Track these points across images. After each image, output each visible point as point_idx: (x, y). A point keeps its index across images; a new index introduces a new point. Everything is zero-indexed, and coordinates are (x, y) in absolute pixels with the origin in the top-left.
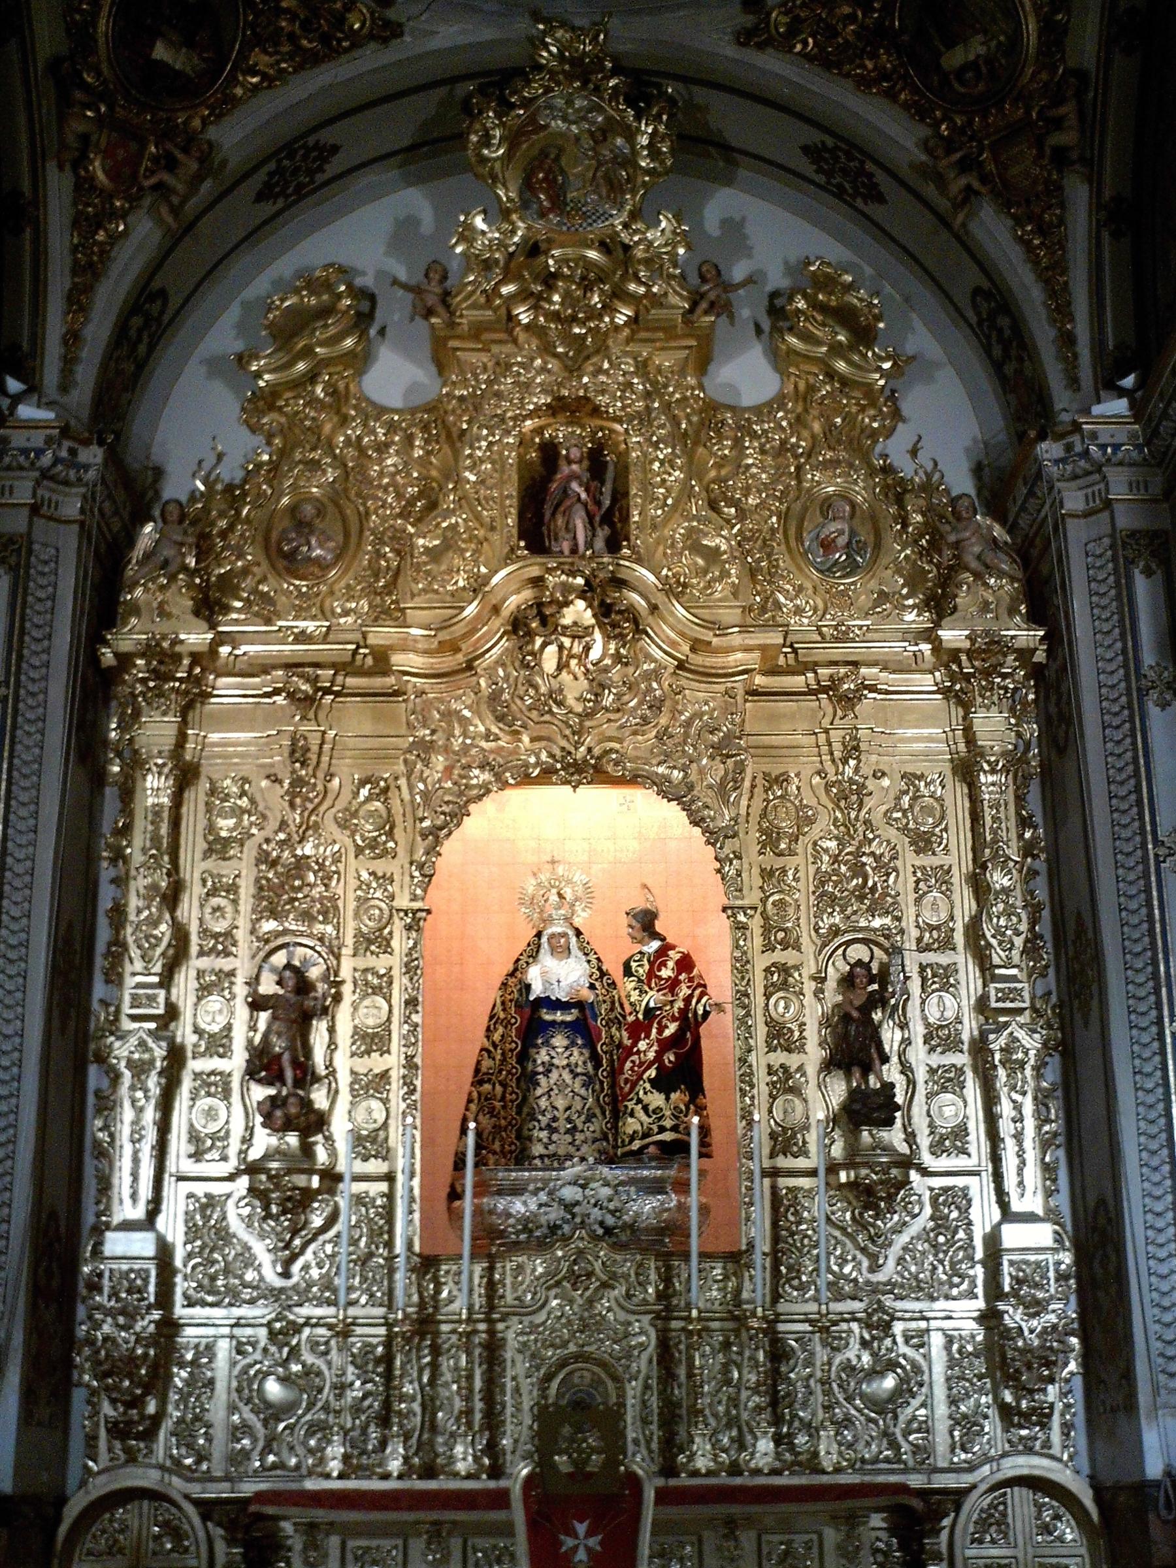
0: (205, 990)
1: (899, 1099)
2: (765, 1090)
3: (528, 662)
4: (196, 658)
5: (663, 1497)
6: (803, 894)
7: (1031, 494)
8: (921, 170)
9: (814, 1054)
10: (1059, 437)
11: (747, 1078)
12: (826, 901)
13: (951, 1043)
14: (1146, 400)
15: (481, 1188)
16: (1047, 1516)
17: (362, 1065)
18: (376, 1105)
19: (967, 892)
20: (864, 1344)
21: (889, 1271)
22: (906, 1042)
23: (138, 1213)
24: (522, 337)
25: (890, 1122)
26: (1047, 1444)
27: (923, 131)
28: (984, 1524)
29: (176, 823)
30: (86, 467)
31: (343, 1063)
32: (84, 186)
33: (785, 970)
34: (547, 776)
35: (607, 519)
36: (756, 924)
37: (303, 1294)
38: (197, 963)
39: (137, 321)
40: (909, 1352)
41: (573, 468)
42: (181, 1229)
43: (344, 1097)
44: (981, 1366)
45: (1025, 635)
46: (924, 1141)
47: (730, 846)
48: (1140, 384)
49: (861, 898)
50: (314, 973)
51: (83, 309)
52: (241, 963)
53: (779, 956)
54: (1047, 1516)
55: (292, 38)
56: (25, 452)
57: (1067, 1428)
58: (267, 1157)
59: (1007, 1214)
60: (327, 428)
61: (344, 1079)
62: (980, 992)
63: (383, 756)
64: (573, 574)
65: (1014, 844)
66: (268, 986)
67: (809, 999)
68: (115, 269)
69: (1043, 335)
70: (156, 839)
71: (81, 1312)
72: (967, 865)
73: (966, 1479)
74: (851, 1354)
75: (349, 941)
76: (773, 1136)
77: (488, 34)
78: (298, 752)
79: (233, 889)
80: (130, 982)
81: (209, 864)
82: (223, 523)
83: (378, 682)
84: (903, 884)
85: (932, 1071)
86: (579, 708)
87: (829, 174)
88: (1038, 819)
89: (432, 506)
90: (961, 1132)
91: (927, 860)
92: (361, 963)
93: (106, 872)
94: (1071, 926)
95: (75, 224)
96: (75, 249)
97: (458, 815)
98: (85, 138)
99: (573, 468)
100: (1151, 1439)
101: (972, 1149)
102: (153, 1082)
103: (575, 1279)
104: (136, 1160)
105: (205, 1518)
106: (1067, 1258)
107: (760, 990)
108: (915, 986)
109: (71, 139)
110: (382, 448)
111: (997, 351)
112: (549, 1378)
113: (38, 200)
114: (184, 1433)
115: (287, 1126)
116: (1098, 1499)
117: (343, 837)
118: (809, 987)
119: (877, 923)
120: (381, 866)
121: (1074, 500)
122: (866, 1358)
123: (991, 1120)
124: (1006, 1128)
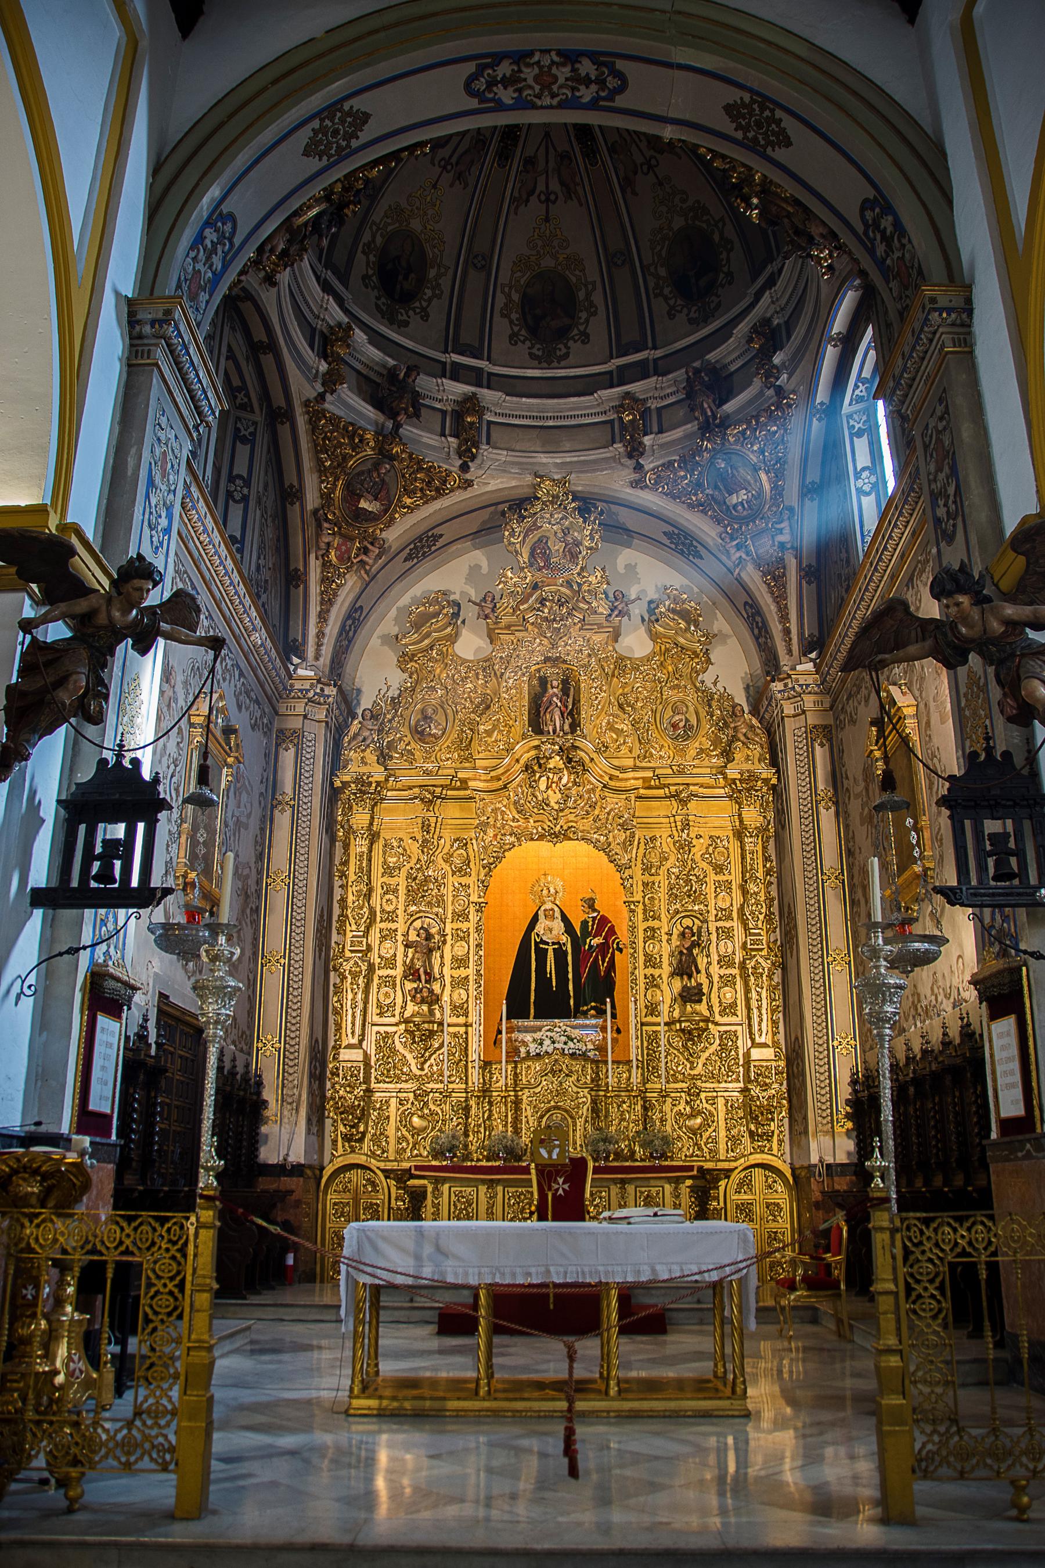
0: (383, 938)
1: (705, 991)
2: (643, 986)
3: (533, 785)
4: (378, 783)
5: (596, 1171)
6: (662, 894)
7: (769, 704)
8: (221, 214)
9: (666, 970)
10: (781, 680)
11: (635, 981)
12: (673, 897)
13: (730, 964)
14: (821, 662)
15: (510, 1030)
16: (770, 1180)
17: (456, 973)
18: (462, 991)
19: (739, 892)
20: (687, 1103)
21: (699, 1069)
22: (709, 963)
23: (355, 1041)
24: (530, 628)
25: (700, 1001)
26: (770, 1149)
27: (720, 529)
28: (741, 1185)
29: (370, 860)
30: (329, 696)
31: (447, 971)
32: (326, 565)
33: (653, 929)
34: (541, 837)
35: (571, 713)
36: (640, 909)
37: (430, 1078)
38: (379, 925)
39: (350, 622)
40: (709, 1107)
41: (554, 690)
42: (374, 1047)
43: (448, 988)
44: (741, 1113)
45: (766, 772)
46: (716, 1009)
47: (628, 872)
48: (819, 656)
49: (689, 896)
50: (433, 931)
51: (326, 620)
52: (400, 926)
53: (651, 923)
54: (770, 1180)
55: (422, 490)
56: (301, 690)
57: (780, 1142)
58: (412, 1015)
59: (754, 1044)
60: (438, 671)
61: (448, 980)
62: (768, 315)
63: (465, 828)
64: (553, 744)
65: (761, 870)
66: (413, 937)
67: (664, 943)
68: (340, 600)
69: (776, 628)
70: (361, 868)
71: (328, 1085)
72: (739, 881)
73: (733, 1165)
74: (681, 1107)
75: (450, 916)
76: (646, 1007)
77: (514, 483)
78: (426, 827)
79: (395, 891)
80: (349, 935)
81: (385, 879)
82: (389, 716)
83: (462, 793)
84: (710, 889)
85: (721, 977)
86: (556, 807)
87: (676, 545)
88: (773, 857)
89: (488, 707)
90: (733, 1005)
91: (721, 878)
92: (455, 926)
93: (337, 882)
94: (786, 909)
95: (322, 581)
96: (322, 593)
97: (499, 859)
98: (328, 544)
99: (554, 690)
100: (813, 1146)
101: (739, 1013)
102: (361, 981)
103: (553, 1072)
104: (354, 1016)
105: (386, 1177)
106: (782, 1064)
107: (641, 940)
108: (714, 937)
109: (323, 546)
110: (464, 679)
111: (756, 631)
112: (542, 1117)
113: (306, 573)
114: (376, 1140)
115: (423, 1001)
116: (793, 1174)
117: (446, 867)
118: (665, 938)
119: (696, 908)
120: (464, 880)
121: (789, 709)
122: (688, 1109)
123: (748, 1000)
124: (754, 1004)
